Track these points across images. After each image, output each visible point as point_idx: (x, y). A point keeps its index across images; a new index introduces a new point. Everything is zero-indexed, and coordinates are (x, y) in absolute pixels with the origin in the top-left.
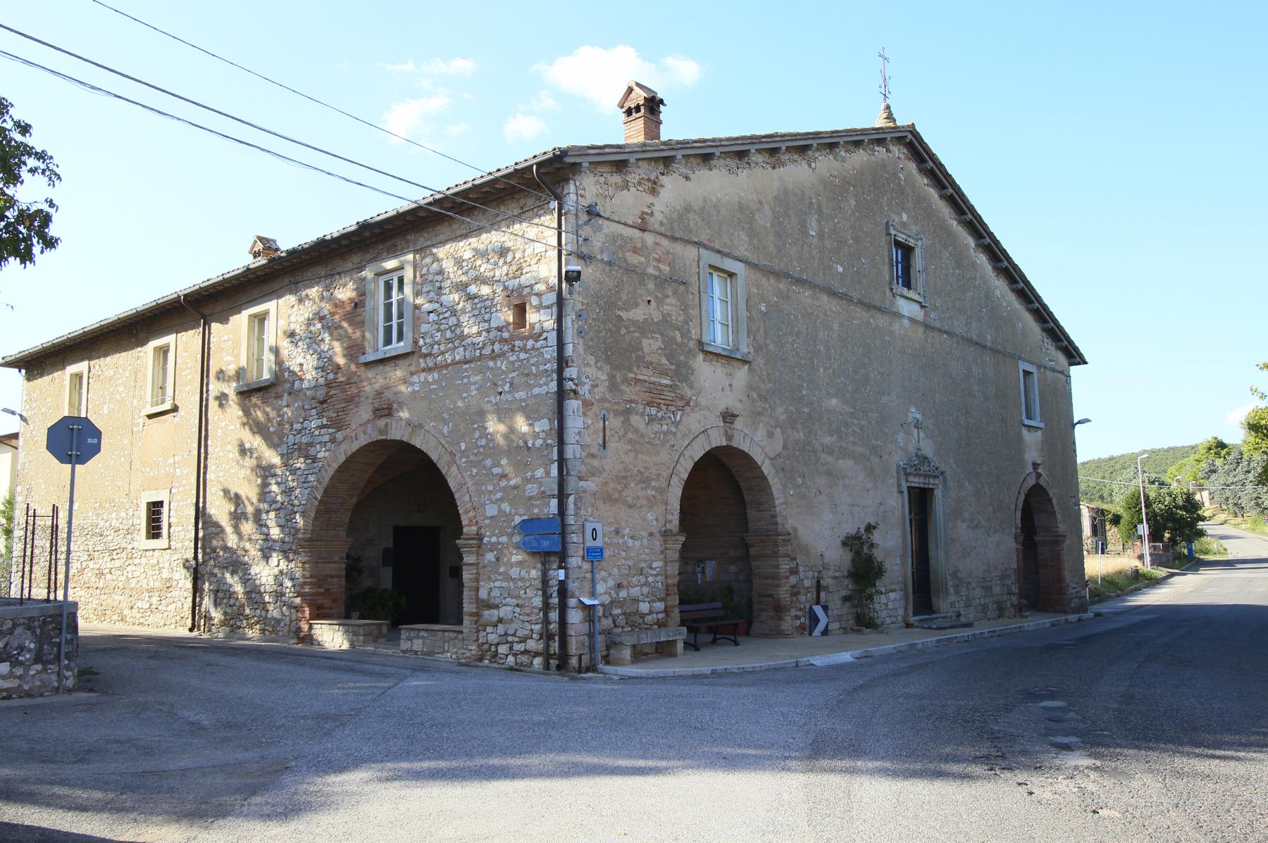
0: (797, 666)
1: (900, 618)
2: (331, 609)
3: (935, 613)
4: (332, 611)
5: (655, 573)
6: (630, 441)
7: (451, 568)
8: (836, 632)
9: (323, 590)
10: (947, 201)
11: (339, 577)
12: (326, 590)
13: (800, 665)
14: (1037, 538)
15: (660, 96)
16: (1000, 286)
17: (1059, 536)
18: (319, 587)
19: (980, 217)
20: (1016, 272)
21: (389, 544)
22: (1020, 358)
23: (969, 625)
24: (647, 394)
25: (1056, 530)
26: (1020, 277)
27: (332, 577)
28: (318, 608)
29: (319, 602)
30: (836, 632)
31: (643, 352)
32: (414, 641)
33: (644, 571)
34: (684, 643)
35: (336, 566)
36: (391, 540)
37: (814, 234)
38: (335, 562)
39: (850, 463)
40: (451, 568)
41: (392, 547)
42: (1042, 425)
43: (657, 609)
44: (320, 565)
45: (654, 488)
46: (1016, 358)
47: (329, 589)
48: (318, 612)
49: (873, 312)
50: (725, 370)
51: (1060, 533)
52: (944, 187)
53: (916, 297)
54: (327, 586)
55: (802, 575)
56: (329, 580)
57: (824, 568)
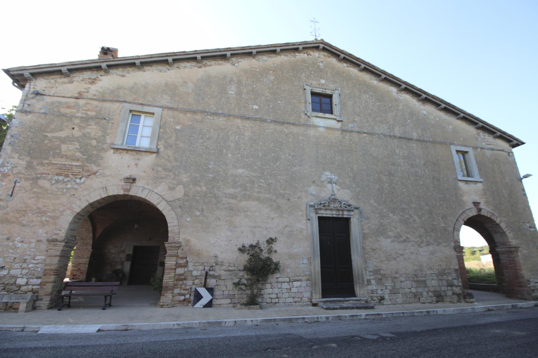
0: (23, 331)
1: (306, 299)
2: (80, 276)
3: (355, 296)
4: (80, 277)
5: (36, 262)
6: (35, 192)
7: (160, 262)
8: (225, 306)
9: (77, 269)
10: (364, 71)
11: (85, 264)
12: (78, 269)
13: (25, 330)
14: (498, 250)
15: (100, 50)
16: (428, 109)
17: (511, 248)
18: (75, 267)
19: (392, 75)
20: (436, 99)
21: (131, 253)
22: (451, 144)
23: (372, 308)
24: (57, 170)
25: (508, 243)
26: (440, 101)
27: (82, 264)
28: (74, 276)
29: (74, 273)
30: (225, 306)
31: (61, 151)
32: (451, 291)
33: (28, 261)
34: (7, 302)
35: (84, 260)
36: (132, 251)
37: (233, 93)
38: (85, 258)
39: (254, 203)
40: (160, 262)
41: (131, 253)
42: (481, 180)
43: (33, 283)
44: (77, 259)
45: (49, 217)
46: (447, 144)
47: (80, 269)
48: (73, 277)
49: (286, 125)
50: (133, 157)
51: (512, 246)
52: (359, 66)
53: (335, 117)
54: (79, 267)
55: (191, 267)
56: (81, 265)
57: (217, 264)
